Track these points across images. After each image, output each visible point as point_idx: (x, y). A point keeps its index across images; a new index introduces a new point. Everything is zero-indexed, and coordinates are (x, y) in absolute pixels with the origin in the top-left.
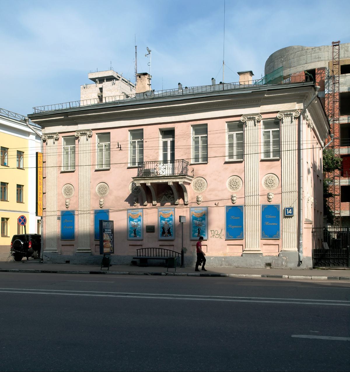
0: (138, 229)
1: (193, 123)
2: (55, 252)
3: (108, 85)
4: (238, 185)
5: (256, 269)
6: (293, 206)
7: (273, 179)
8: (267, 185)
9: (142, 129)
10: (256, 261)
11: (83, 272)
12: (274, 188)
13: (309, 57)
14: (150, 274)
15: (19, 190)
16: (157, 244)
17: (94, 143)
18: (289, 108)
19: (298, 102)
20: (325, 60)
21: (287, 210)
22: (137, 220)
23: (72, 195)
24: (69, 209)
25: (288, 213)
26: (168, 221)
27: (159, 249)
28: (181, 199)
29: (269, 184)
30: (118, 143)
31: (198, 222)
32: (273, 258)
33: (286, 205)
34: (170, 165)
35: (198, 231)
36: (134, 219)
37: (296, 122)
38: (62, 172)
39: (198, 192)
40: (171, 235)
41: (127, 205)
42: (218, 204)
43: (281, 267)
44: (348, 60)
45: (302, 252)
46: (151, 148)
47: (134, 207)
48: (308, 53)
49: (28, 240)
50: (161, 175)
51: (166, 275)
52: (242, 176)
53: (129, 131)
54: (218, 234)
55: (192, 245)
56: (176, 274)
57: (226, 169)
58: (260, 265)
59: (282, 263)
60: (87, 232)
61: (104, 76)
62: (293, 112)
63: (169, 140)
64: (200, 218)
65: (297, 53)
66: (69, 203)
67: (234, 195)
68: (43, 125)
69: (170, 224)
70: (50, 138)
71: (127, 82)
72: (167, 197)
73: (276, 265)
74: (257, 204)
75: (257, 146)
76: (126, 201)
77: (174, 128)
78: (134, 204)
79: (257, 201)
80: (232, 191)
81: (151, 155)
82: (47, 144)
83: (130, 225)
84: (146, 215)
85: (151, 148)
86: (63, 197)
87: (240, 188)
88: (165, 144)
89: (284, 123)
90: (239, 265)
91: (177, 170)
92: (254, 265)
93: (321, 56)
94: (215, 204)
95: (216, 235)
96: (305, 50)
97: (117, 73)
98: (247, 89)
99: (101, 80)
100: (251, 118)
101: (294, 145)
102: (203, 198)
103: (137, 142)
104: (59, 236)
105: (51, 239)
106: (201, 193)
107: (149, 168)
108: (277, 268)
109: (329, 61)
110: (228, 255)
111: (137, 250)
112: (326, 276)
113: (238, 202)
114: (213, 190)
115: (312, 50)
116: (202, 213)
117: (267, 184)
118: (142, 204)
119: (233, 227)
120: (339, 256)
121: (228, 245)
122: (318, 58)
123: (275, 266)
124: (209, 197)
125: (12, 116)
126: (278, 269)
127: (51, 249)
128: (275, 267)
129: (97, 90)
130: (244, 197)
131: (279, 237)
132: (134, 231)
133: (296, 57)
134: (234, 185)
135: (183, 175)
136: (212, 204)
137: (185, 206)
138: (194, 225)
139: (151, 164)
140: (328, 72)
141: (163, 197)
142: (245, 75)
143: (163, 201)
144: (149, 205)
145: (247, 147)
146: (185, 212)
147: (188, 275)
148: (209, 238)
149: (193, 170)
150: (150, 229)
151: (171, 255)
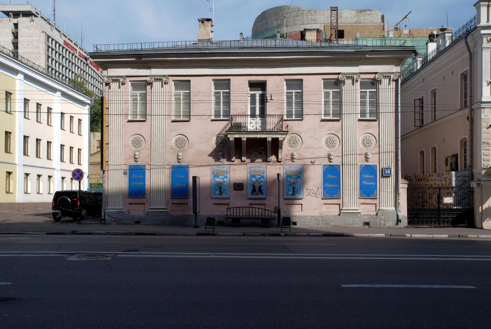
0: (225, 186)
1: (287, 77)
2: (121, 212)
3: (26, 21)
4: (335, 144)
5: (357, 228)
6: (390, 166)
7: (370, 139)
8: (364, 145)
9: (229, 80)
10: (354, 220)
11: (189, 234)
12: (371, 148)
13: (305, 18)
14: (268, 235)
15: (7, 137)
16: (246, 203)
17: (171, 92)
18: (387, 71)
19: (397, 65)
20: (321, 23)
21: (386, 170)
22: (223, 177)
23: (142, 148)
24: (139, 163)
25: (386, 173)
26: (260, 179)
27: (249, 207)
28: (274, 155)
29: (366, 144)
30: (271, 95)
31: (293, 180)
32: (371, 217)
33: (383, 165)
34: (258, 120)
35: (292, 189)
36: (220, 176)
37: (393, 84)
38: (129, 121)
39: (293, 149)
40: (262, 193)
41: (211, 160)
42: (314, 162)
43: (380, 226)
44: (342, 25)
45: (400, 211)
46: (239, 101)
47: (219, 163)
48: (304, 15)
49: (76, 197)
50: (258, 130)
51: (285, 236)
52: (340, 135)
53: (213, 80)
54: (314, 193)
55: (286, 204)
56: (297, 234)
57: (323, 127)
58: (358, 224)
59: (380, 222)
60: (162, 189)
61: (20, 10)
62: (391, 74)
63: (258, 93)
64: (294, 176)
65: (293, 13)
66: (138, 156)
67: (332, 154)
68: (105, 66)
69: (261, 181)
70: (114, 81)
71: (46, 20)
72: (258, 153)
73: (374, 224)
74: (355, 164)
75: (355, 106)
76: (210, 155)
77: (266, 80)
78: (220, 159)
79: (355, 160)
80: (328, 149)
81: (239, 108)
82: (110, 88)
83: (215, 182)
84: (234, 172)
85: (239, 101)
86: (130, 149)
87: (337, 146)
88: (253, 97)
89: (382, 84)
90: (336, 224)
91: (269, 126)
92: (352, 224)
93: (317, 19)
94: (312, 162)
95: (311, 194)
96: (301, 11)
97: (35, 8)
98: (350, 48)
99: (16, 14)
100: (350, 77)
101: (392, 107)
102: (298, 155)
103: (221, 92)
104: (126, 193)
105: (116, 195)
106: (296, 150)
107: (240, 122)
108: (375, 227)
109: (324, 24)
110: (325, 214)
112: (447, 234)
113: (336, 161)
114: (309, 148)
115: (308, 11)
116: (297, 171)
117: (364, 143)
118: (229, 160)
119: (330, 186)
120: (435, 215)
121: (324, 204)
122: (314, 20)
123: (373, 225)
124: (304, 155)
126: (376, 228)
127: (115, 208)
128: (373, 226)
129: (11, 25)
130: (341, 155)
131: (376, 196)
132: (220, 188)
133: (292, 17)
135: (280, 131)
136: (308, 162)
137: (279, 164)
138: (289, 183)
139: (242, 118)
140: (325, 35)
141: (254, 153)
142: (312, 32)
143: (253, 157)
144: (237, 161)
145: (345, 106)
146: (278, 170)
147: (309, 236)
148: (305, 197)
149: (287, 126)
150: (238, 186)
151: (263, 214)
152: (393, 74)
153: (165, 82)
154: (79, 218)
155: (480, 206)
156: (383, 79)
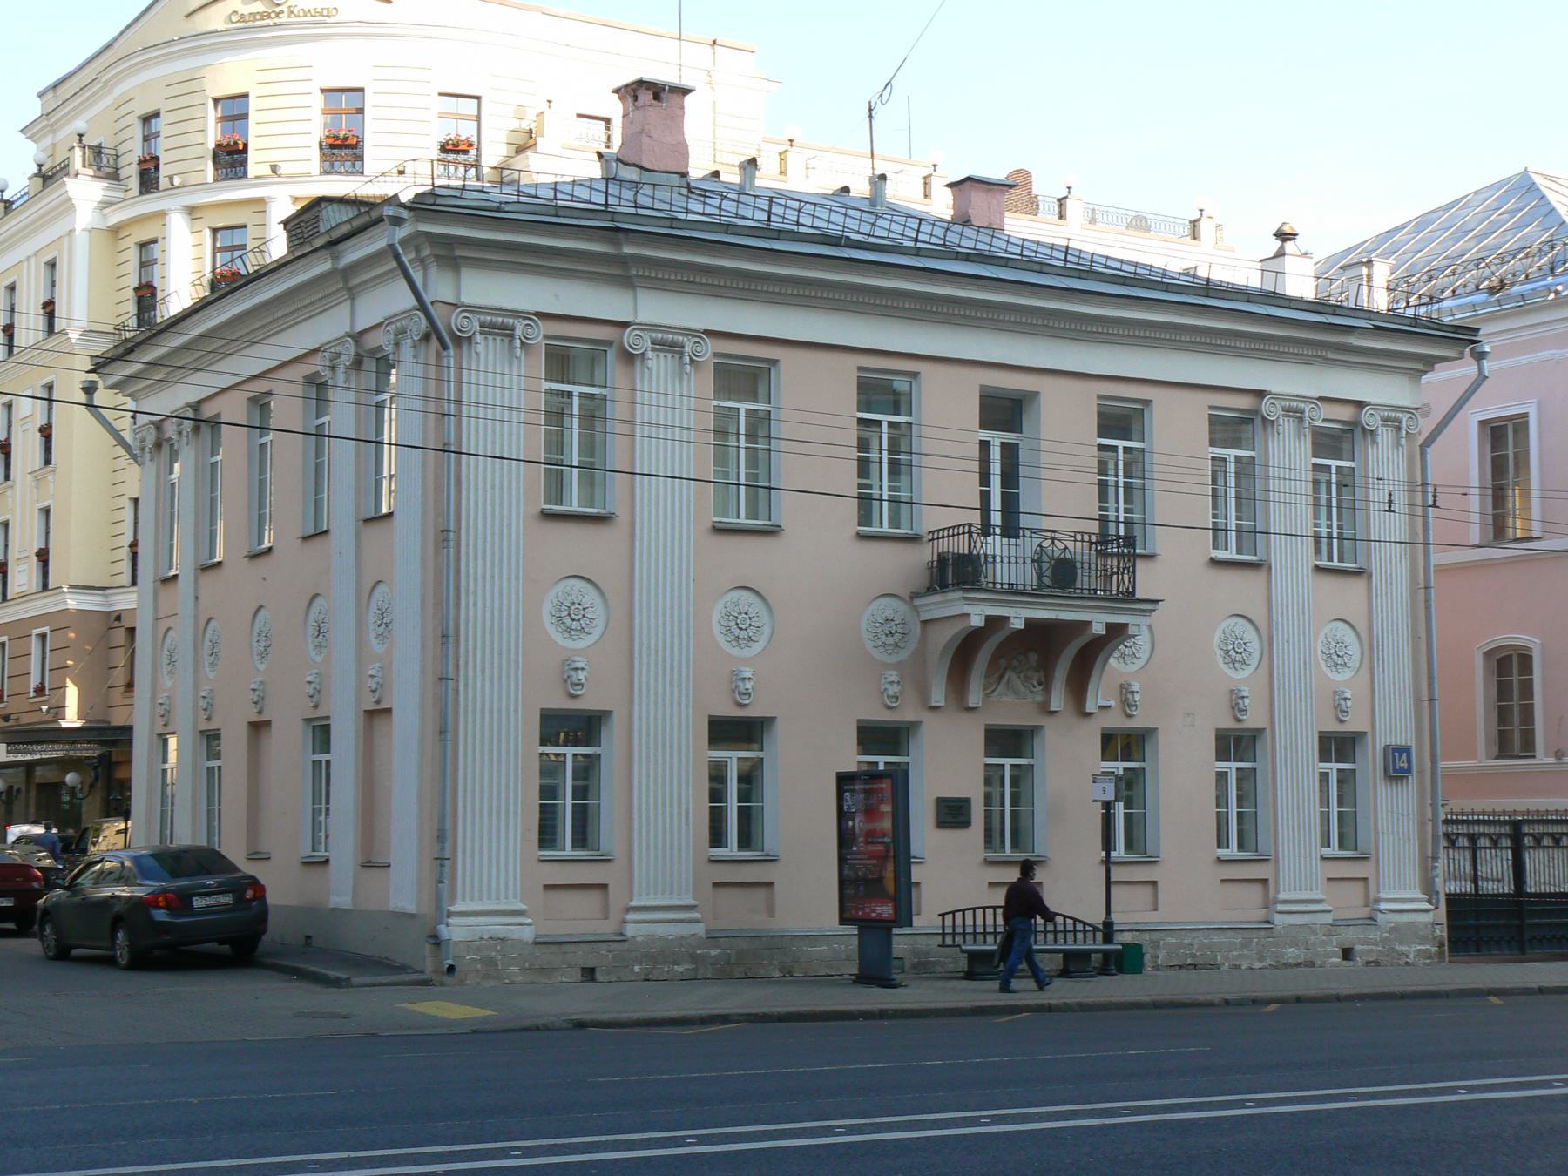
52: (1262, 623)
62: (518, 317)
111: (942, 915)
125: (1411, 255)
134: (573, 616)
153: (525, 340)
155: (16, 925)
156: (1385, 429)
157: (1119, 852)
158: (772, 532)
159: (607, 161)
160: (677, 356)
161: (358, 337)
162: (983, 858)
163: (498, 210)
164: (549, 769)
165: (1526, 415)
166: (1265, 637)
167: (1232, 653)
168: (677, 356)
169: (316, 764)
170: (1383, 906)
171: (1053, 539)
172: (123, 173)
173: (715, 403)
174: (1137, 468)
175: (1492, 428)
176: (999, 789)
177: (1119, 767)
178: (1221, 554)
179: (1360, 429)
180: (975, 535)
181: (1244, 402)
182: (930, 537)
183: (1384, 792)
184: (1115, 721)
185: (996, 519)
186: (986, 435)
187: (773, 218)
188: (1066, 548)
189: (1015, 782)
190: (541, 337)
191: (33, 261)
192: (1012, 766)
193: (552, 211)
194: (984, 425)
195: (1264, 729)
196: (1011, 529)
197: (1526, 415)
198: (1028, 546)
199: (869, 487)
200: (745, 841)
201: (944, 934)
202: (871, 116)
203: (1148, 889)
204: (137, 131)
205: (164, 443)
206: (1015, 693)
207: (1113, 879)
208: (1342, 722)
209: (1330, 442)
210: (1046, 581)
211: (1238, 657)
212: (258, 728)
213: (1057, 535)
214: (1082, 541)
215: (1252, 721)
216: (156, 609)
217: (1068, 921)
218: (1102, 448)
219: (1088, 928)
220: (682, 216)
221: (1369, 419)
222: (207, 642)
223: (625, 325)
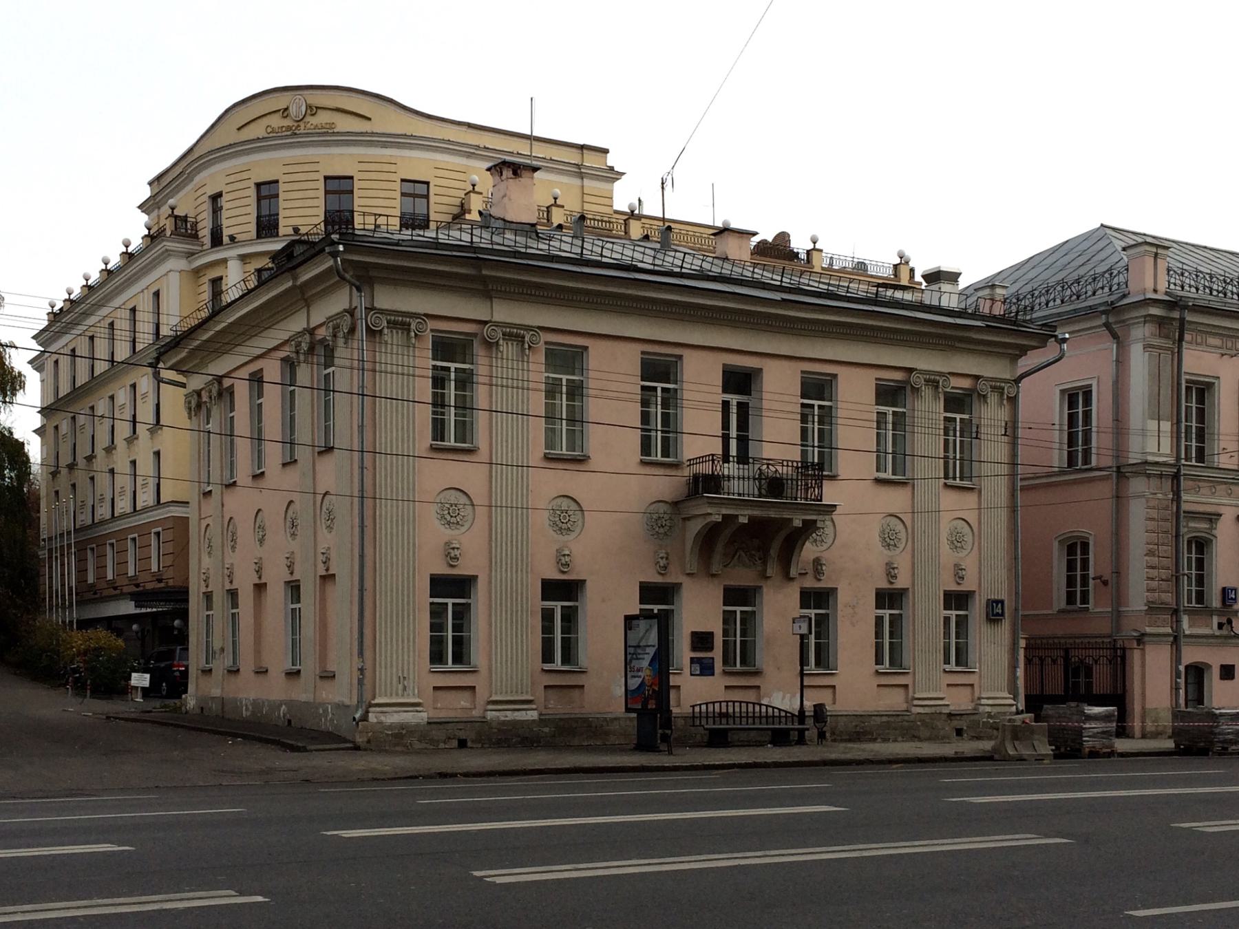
111: (693, 707)
152: (417, 318)
154: (1182, 747)
157: (811, 667)
158: (582, 460)
159: (485, 217)
160: (520, 344)
161: (311, 331)
162: (874, 671)
163: (397, 245)
164: (547, 616)
165: (1090, 386)
166: (910, 531)
167: (887, 539)
168: (520, 344)
169: (293, 610)
170: (984, 702)
171: (768, 464)
172: (201, 234)
173: (546, 375)
174: (827, 420)
175: (1069, 395)
176: (733, 626)
177: (812, 613)
178: (882, 475)
179: (976, 394)
180: (716, 462)
181: (898, 376)
182: (688, 463)
183: (986, 629)
184: (809, 583)
185: (733, 451)
186: (728, 397)
187: (585, 252)
188: (777, 470)
189: (743, 622)
190: (428, 330)
191: (146, 291)
192: (741, 612)
193: (434, 246)
194: (725, 390)
195: (908, 589)
196: (743, 458)
197: (1090, 386)
198: (751, 470)
199: (650, 430)
200: (566, 659)
201: (694, 717)
202: (663, 188)
203: (830, 691)
204: (207, 207)
205: (203, 405)
206: (744, 565)
207: (805, 684)
208: (959, 584)
209: (956, 402)
210: (763, 492)
211: (892, 542)
212: (260, 588)
213: (771, 462)
214: (788, 466)
215: (900, 583)
216: (200, 515)
217: (775, 710)
218: (803, 405)
219: (788, 715)
220: (523, 250)
221: (983, 387)
222: (230, 534)
223: (485, 323)
